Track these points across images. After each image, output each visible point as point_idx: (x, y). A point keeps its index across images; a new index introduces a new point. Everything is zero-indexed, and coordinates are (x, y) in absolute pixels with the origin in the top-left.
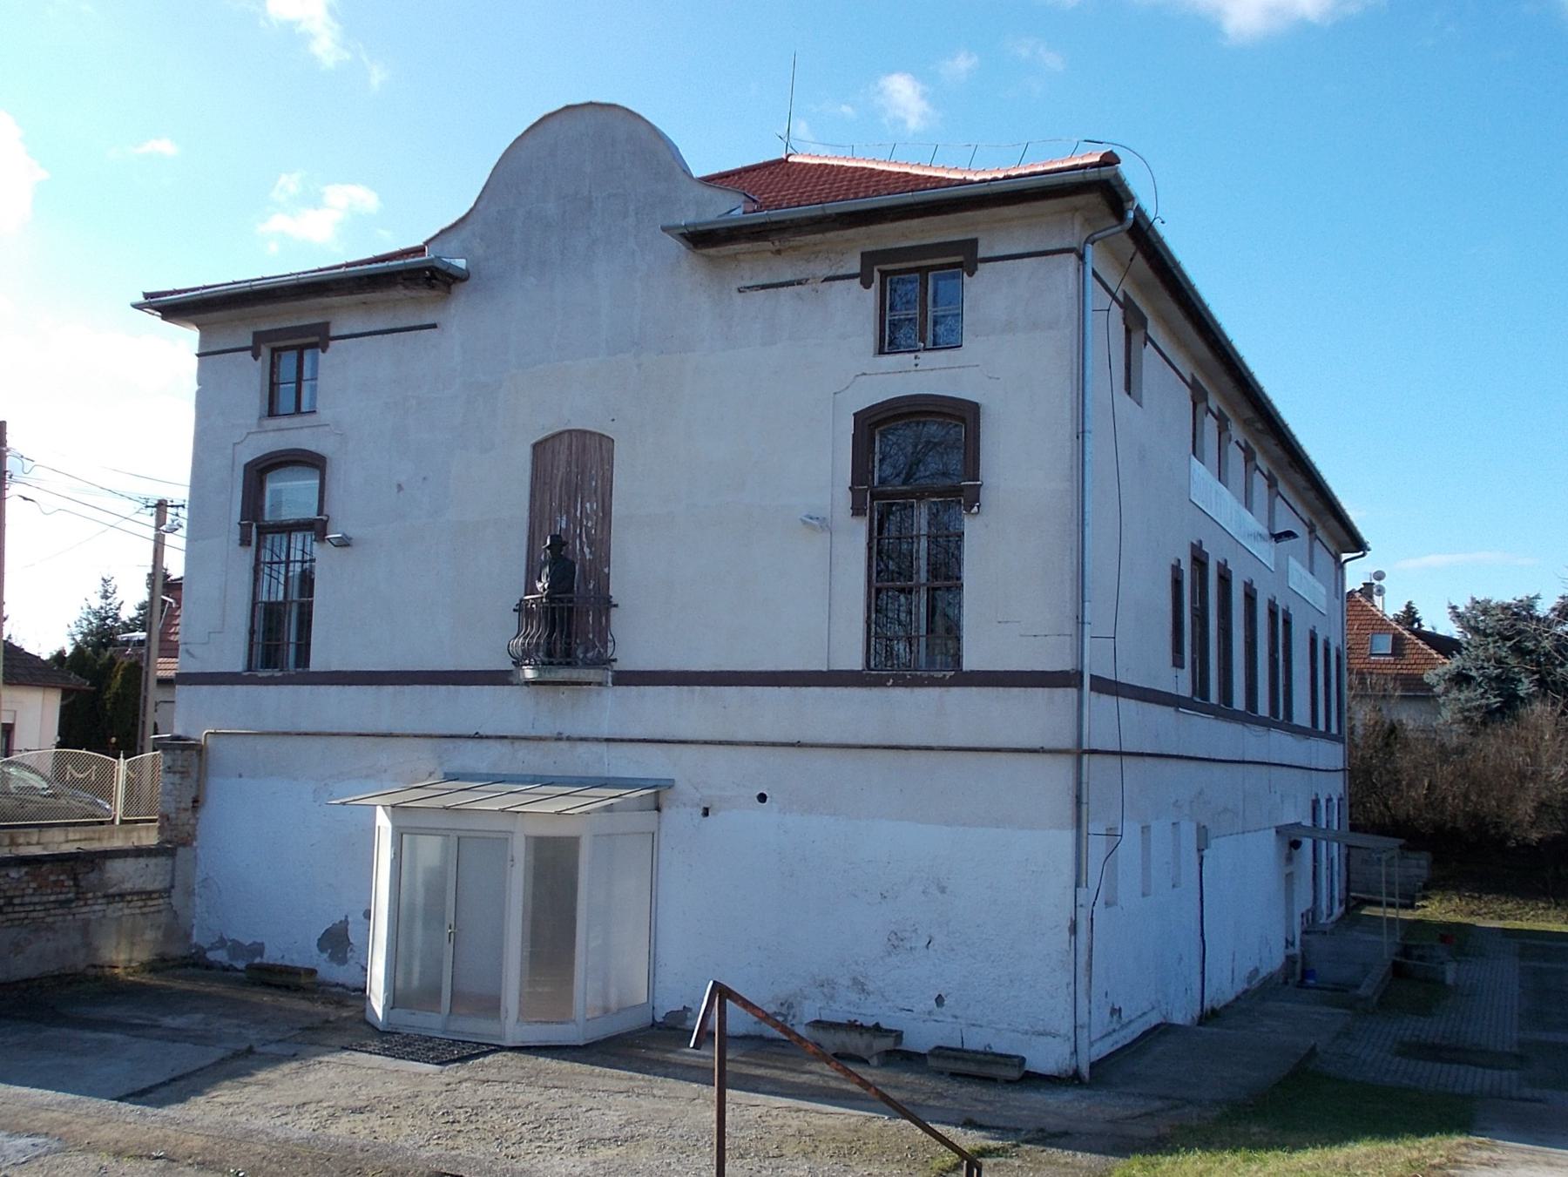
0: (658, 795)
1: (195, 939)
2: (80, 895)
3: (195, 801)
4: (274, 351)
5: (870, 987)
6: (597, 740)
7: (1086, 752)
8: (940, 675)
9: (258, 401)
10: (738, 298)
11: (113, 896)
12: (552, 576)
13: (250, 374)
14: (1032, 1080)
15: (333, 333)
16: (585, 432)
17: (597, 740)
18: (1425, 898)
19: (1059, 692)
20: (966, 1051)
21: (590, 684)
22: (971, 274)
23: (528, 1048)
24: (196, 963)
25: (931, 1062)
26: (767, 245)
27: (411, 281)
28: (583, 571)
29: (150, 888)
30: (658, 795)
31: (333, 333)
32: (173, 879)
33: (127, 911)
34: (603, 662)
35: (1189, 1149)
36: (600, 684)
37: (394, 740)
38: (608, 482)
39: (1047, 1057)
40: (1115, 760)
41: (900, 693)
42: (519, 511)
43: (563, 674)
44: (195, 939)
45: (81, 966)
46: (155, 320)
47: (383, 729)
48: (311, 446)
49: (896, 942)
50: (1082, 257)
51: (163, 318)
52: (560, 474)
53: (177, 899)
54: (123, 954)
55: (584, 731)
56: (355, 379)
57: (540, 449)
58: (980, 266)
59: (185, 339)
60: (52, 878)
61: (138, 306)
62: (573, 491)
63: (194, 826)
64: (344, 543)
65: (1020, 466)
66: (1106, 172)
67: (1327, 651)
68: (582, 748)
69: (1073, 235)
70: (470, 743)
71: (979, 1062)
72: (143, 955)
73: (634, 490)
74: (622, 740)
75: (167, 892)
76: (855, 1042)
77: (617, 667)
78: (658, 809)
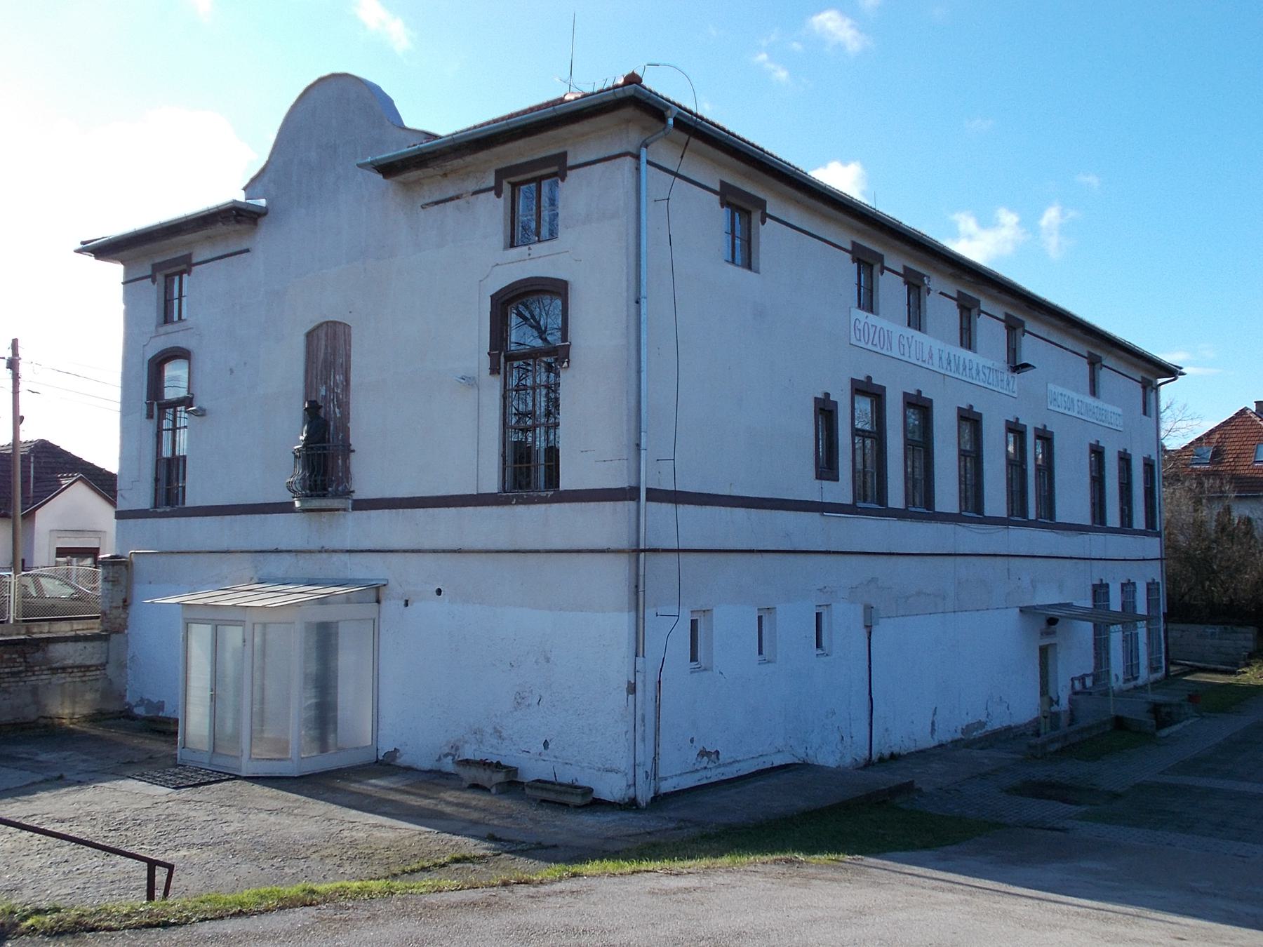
0: (376, 592)
1: (128, 699)
2: (29, 668)
3: (125, 601)
4: (167, 276)
5: (504, 734)
6: (342, 551)
7: (644, 551)
8: (543, 494)
9: (155, 315)
10: (422, 213)
11: (57, 669)
12: (308, 432)
13: (151, 292)
14: (595, 804)
15: (194, 261)
16: (335, 323)
17: (342, 551)
18: (1248, 665)
19: (620, 504)
20: (561, 785)
21: (338, 510)
22: (563, 180)
23: (258, 778)
24: (126, 716)
25: (528, 791)
26: (429, 171)
27: (234, 219)
28: (336, 427)
29: (88, 663)
30: (376, 592)
31: (194, 261)
32: (107, 657)
33: (69, 679)
34: (348, 493)
35: (593, 860)
36: (345, 510)
37: (230, 556)
38: (348, 356)
39: (611, 788)
40: (674, 556)
41: (521, 509)
42: (300, 385)
43: (316, 503)
44: (128, 699)
45: (33, 717)
46: (90, 259)
47: (224, 547)
48: (182, 344)
49: (520, 701)
50: (637, 157)
51: (97, 257)
52: (321, 355)
53: (111, 670)
54: (67, 708)
55: (337, 546)
56: (203, 291)
57: (310, 335)
58: (569, 173)
59: (114, 271)
60: (6, 656)
61: (79, 251)
62: (329, 365)
63: (125, 619)
64: (201, 413)
65: (595, 328)
66: (630, 90)
67: (972, 458)
68: (336, 558)
69: (631, 139)
70: (273, 556)
71: (557, 792)
72: (82, 710)
73: (365, 365)
74: (405, 551)
75: (103, 666)
76: (482, 776)
77: (355, 496)
78: (378, 601)
